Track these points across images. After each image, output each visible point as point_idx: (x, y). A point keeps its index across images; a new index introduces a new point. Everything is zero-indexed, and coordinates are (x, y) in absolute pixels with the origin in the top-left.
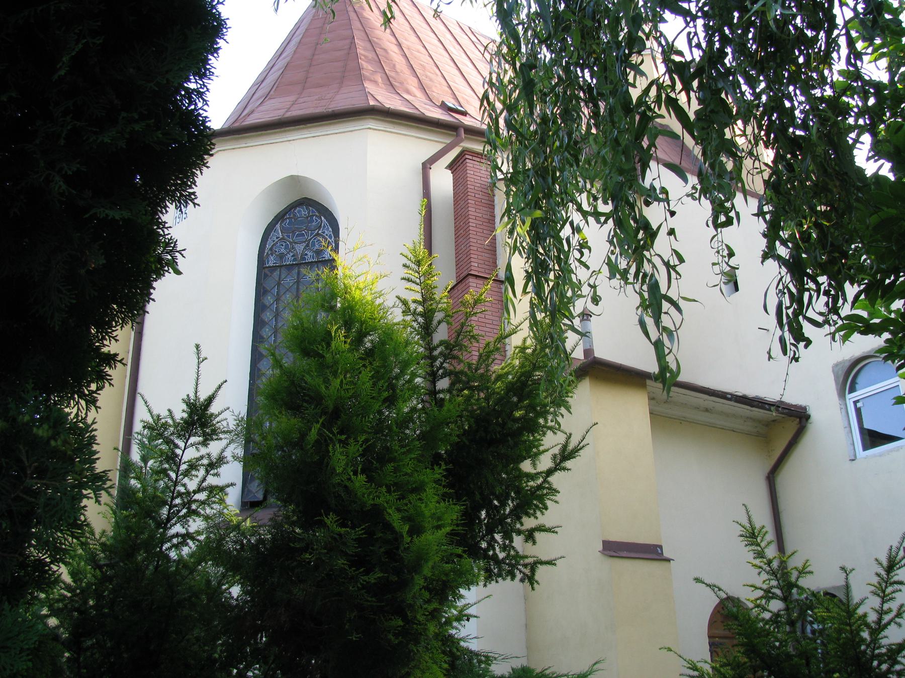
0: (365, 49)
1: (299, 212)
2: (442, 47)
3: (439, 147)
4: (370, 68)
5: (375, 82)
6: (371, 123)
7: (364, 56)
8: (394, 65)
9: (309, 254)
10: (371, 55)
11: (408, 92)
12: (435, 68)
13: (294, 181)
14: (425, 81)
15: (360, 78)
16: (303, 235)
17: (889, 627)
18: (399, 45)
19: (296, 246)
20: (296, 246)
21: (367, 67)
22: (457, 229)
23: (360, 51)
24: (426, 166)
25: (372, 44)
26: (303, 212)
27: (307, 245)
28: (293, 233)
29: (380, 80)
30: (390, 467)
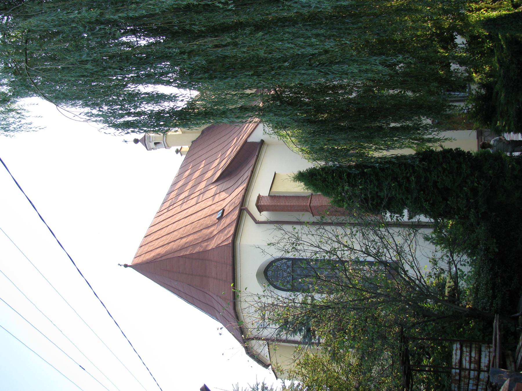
0: (187, 251)
1: (269, 274)
2: (160, 231)
3: (248, 217)
4: (198, 248)
5: (207, 246)
6: (238, 242)
7: (191, 251)
8: (195, 239)
9: (288, 270)
10: (190, 249)
11: (211, 233)
12: (193, 224)
13: (258, 275)
14: (204, 226)
15: (205, 252)
16: (280, 273)
17: (327, 7)
18: (181, 238)
19: (284, 276)
20: (284, 276)
21: (197, 249)
22: (288, 211)
23: (188, 253)
24: (257, 222)
25: (182, 248)
26: (270, 273)
27: (285, 271)
28: (278, 277)
29: (206, 244)
30: (466, 127)
